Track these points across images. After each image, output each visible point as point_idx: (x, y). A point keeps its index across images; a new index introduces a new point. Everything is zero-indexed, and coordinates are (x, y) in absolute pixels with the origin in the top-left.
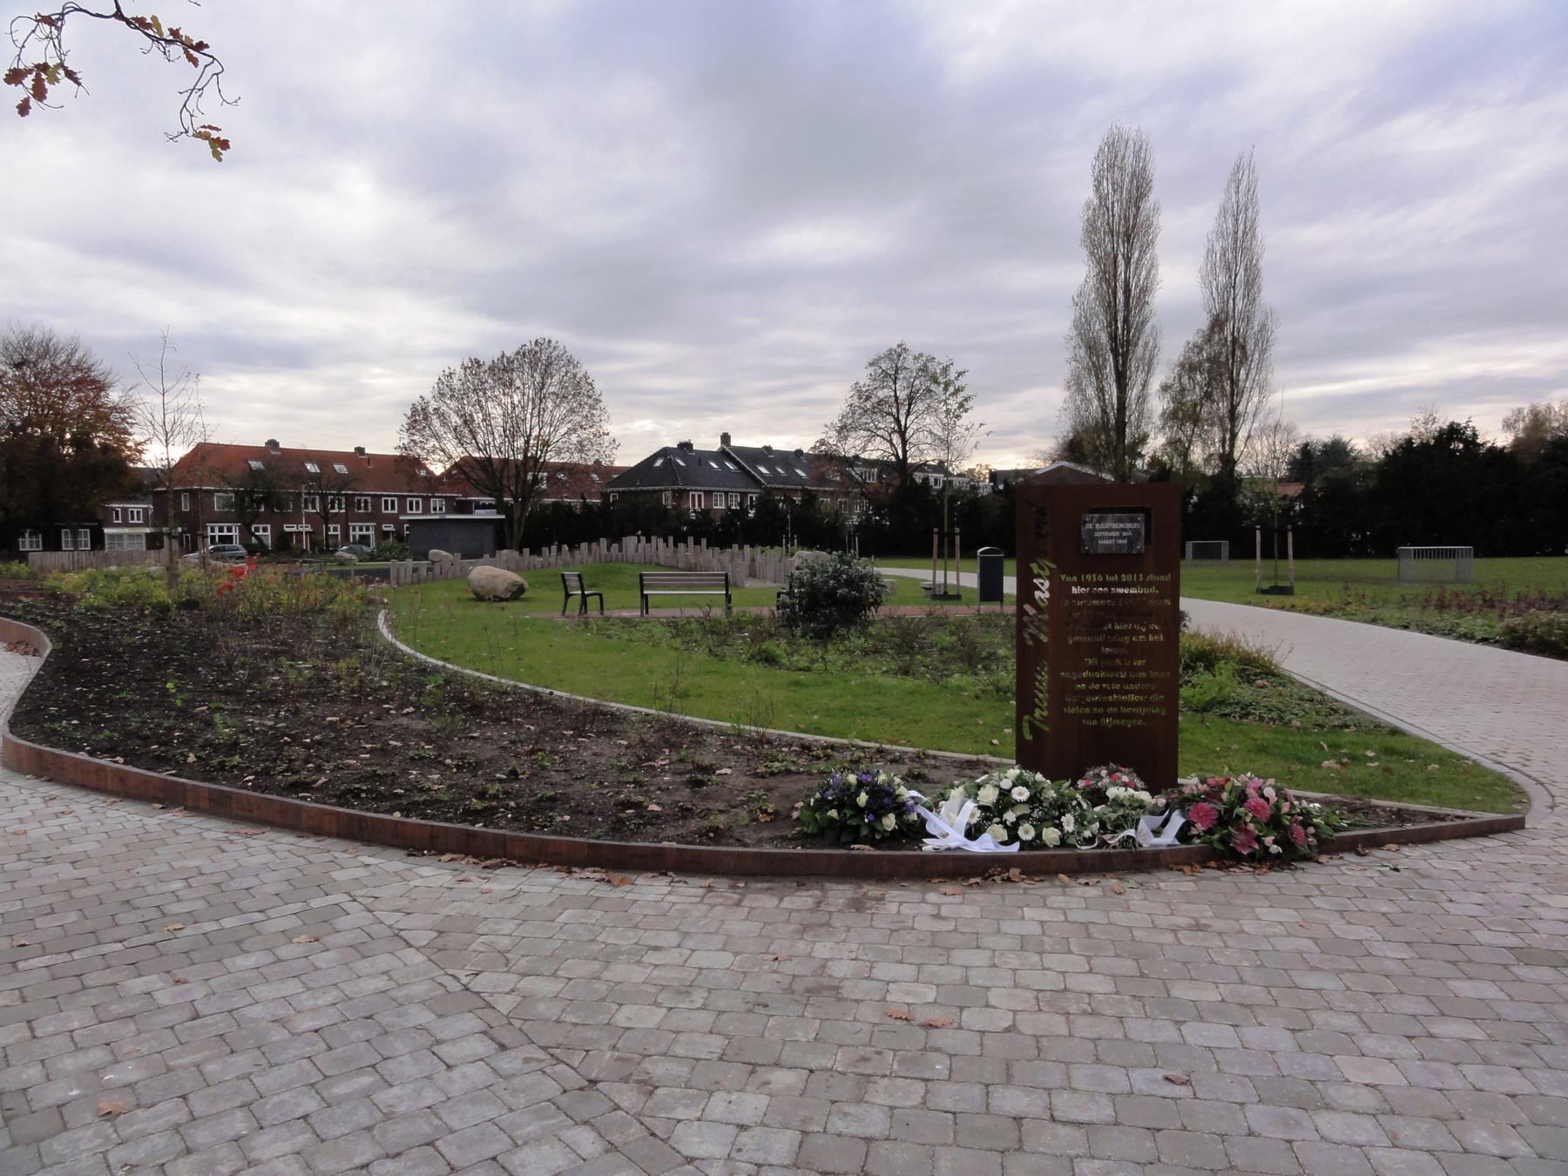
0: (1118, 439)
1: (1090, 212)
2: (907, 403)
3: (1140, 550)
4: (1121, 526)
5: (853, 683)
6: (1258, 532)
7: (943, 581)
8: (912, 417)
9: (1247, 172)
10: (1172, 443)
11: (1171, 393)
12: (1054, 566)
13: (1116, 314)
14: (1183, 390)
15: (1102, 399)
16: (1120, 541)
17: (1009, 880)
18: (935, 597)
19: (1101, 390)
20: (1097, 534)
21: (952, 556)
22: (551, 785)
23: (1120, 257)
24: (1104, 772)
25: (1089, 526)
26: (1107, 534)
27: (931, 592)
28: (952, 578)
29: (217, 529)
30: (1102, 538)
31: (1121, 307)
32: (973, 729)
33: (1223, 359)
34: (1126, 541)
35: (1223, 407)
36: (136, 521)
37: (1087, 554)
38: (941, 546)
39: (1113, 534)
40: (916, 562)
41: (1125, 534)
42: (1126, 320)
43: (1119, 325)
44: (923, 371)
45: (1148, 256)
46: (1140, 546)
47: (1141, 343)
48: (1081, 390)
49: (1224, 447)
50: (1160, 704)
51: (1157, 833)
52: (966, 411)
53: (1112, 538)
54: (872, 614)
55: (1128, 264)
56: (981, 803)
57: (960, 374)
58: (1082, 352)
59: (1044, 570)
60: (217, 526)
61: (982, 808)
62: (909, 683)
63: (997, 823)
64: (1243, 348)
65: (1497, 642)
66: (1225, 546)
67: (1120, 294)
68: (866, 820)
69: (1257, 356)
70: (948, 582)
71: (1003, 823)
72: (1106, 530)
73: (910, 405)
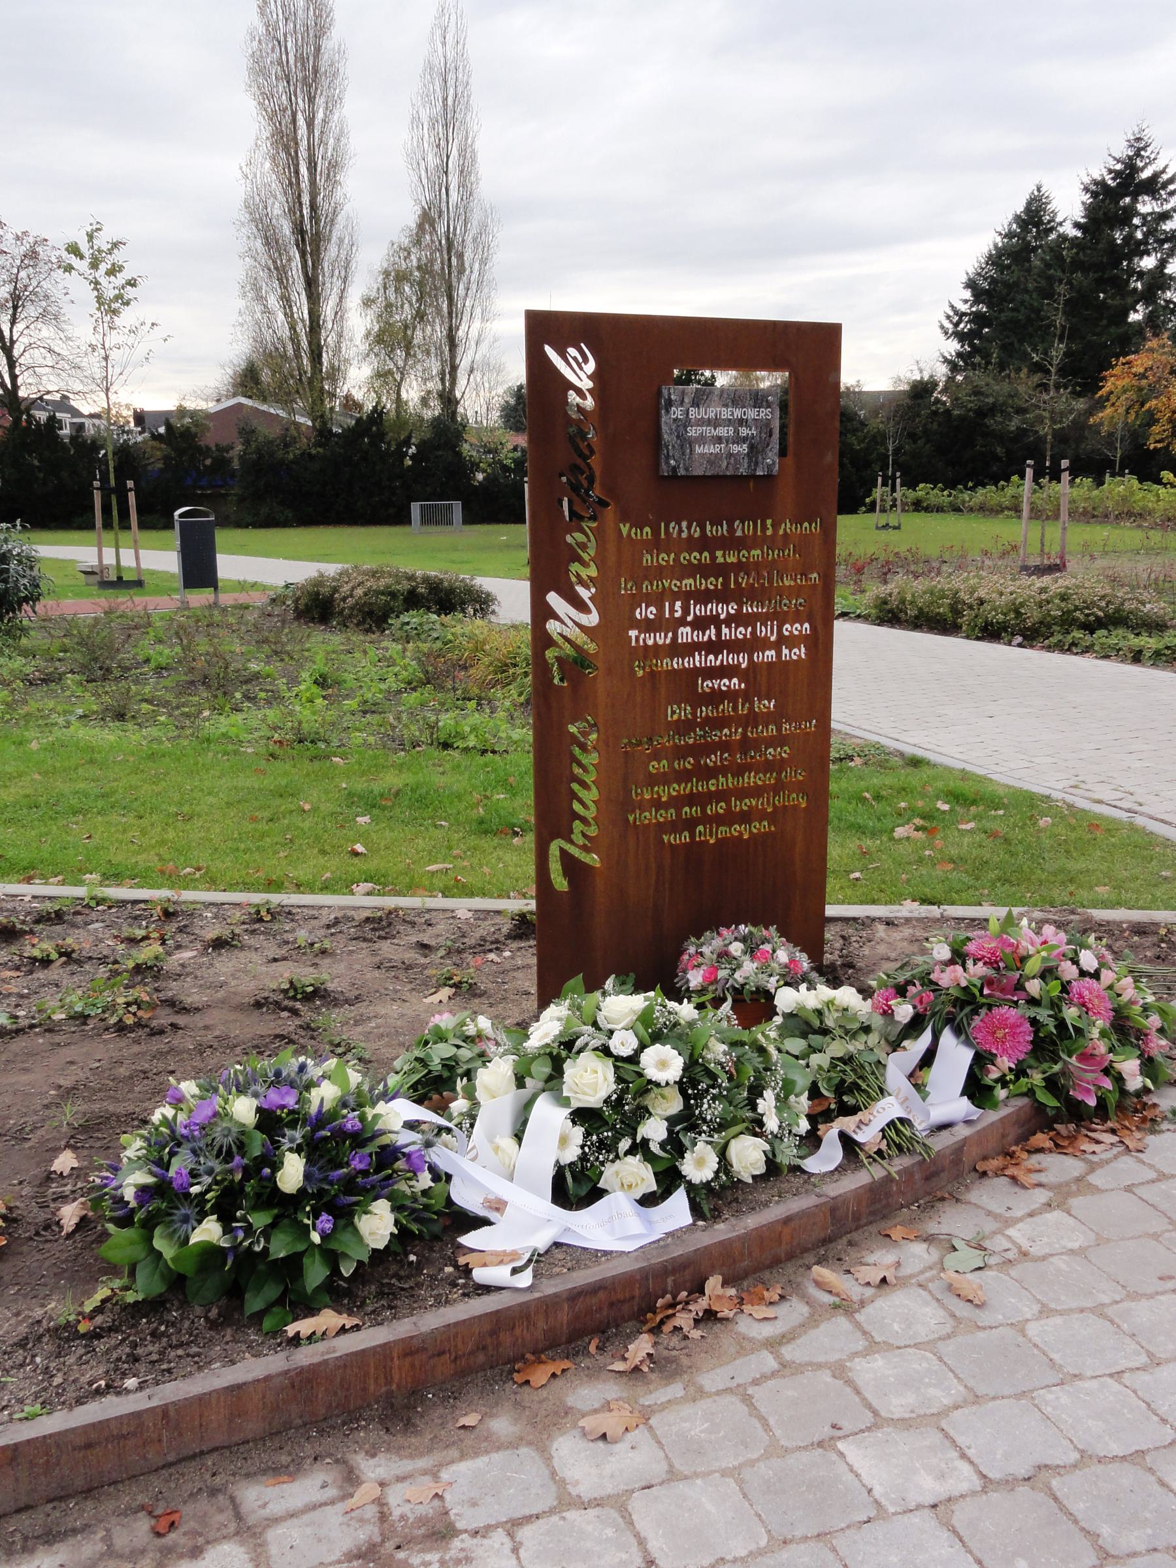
0: (313, 368)
1: (255, 43)
2: (10, 304)
3: (770, 467)
4: (738, 413)
5: (34, 746)
6: (526, 485)
7: (114, 562)
8: (20, 327)
9: (453, 17)
10: (382, 375)
11: (376, 309)
13: (299, 195)
14: (389, 306)
15: (289, 315)
16: (735, 449)
17: (710, 1316)
18: (105, 585)
19: (286, 301)
20: (693, 432)
21: (125, 525)
23: (300, 116)
24: (736, 948)
25: (677, 412)
26: (709, 431)
27: (97, 578)
28: (128, 559)
30: (702, 440)
31: (305, 184)
32: (297, 820)
33: (437, 267)
34: (744, 448)
35: (439, 332)
37: (674, 477)
38: (106, 510)
39: (722, 431)
40: (60, 535)
41: (744, 432)
42: (313, 207)
43: (305, 212)
44: (32, 258)
45: (336, 118)
46: (771, 458)
47: (334, 239)
48: (260, 298)
49: (443, 380)
50: (800, 788)
52: (127, 303)
53: (719, 440)
54: (25, 615)
55: (310, 124)
56: (575, 1104)
57: (115, 245)
58: (259, 244)
61: (582, 1116)
62: (134, 736)
63: (628, 1153)
64: (460, 256)
65: (859, 616)
66: (457, 506)
67: (303, 170)
68: (316, 1238)
69: (476, 266)
70: (123, 563)
71: (641, 1148)
72: (709, 422)
73: (15, 308)
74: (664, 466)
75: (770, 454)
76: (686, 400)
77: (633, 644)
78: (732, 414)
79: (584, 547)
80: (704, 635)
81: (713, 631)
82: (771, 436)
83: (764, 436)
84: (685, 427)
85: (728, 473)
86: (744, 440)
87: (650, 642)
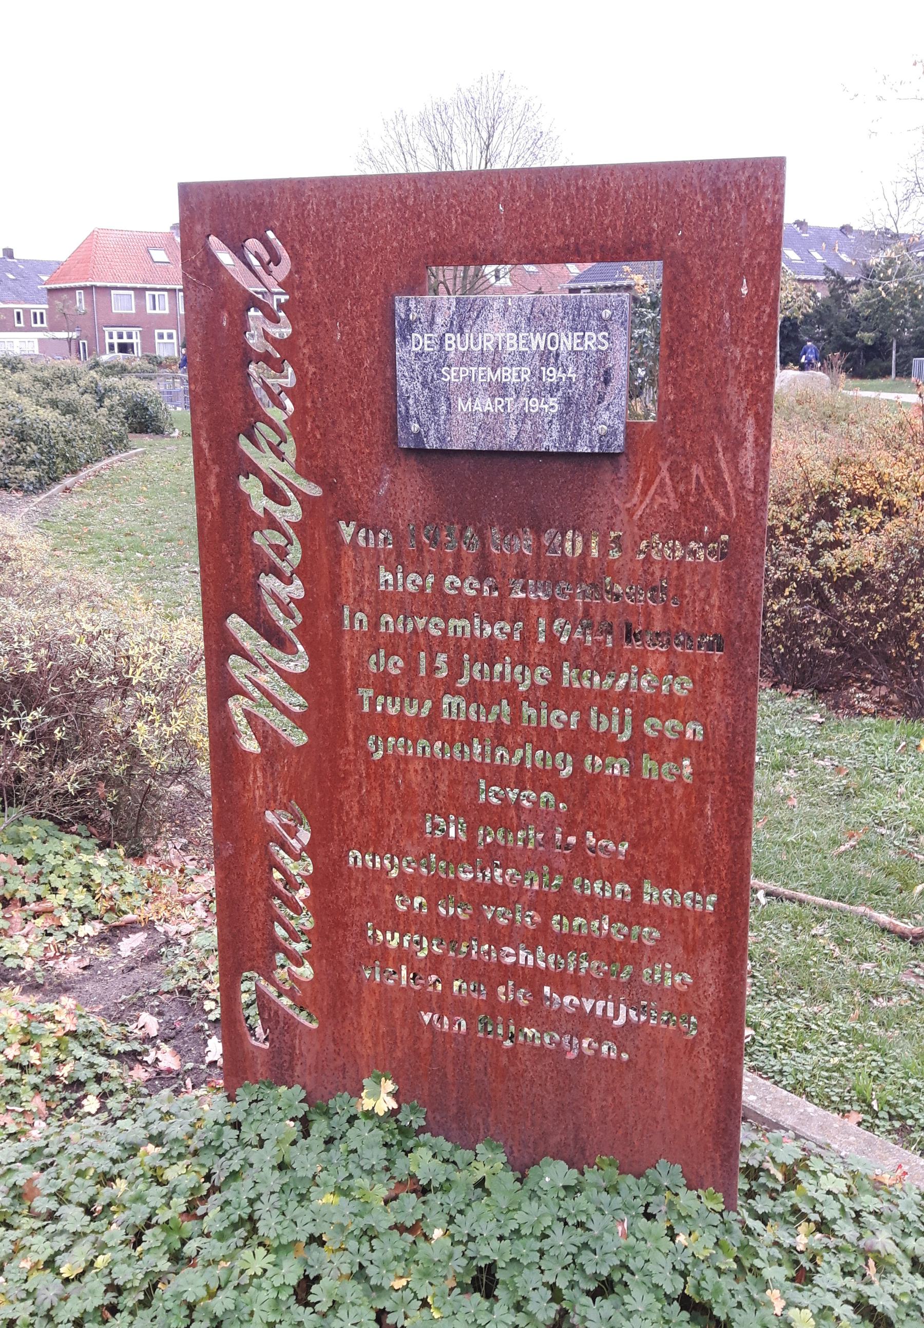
12: (314, 491)
16: (534, 405)
22: (197, 662)
25: (421, 341)
26: (483, 374)
29: (115, 335)
34: (553, 404)
36: (39, 325)
41: (552, 375)
51: (652, 726)
53: (501, 389)
59: (286, 502)
60: (115, 331)
74: (401, 434)
75: (606, 416)
76: (439, 320)
77: (366, 709)
78: (528, 344)
79: (282, 553)
80: (488, 713)
81: (506, 709)
82: (606, 382)
83: (591, 381)
84: (438, 367)
85: (519, 448)
86: (552, 390)
87: (392, 711)
